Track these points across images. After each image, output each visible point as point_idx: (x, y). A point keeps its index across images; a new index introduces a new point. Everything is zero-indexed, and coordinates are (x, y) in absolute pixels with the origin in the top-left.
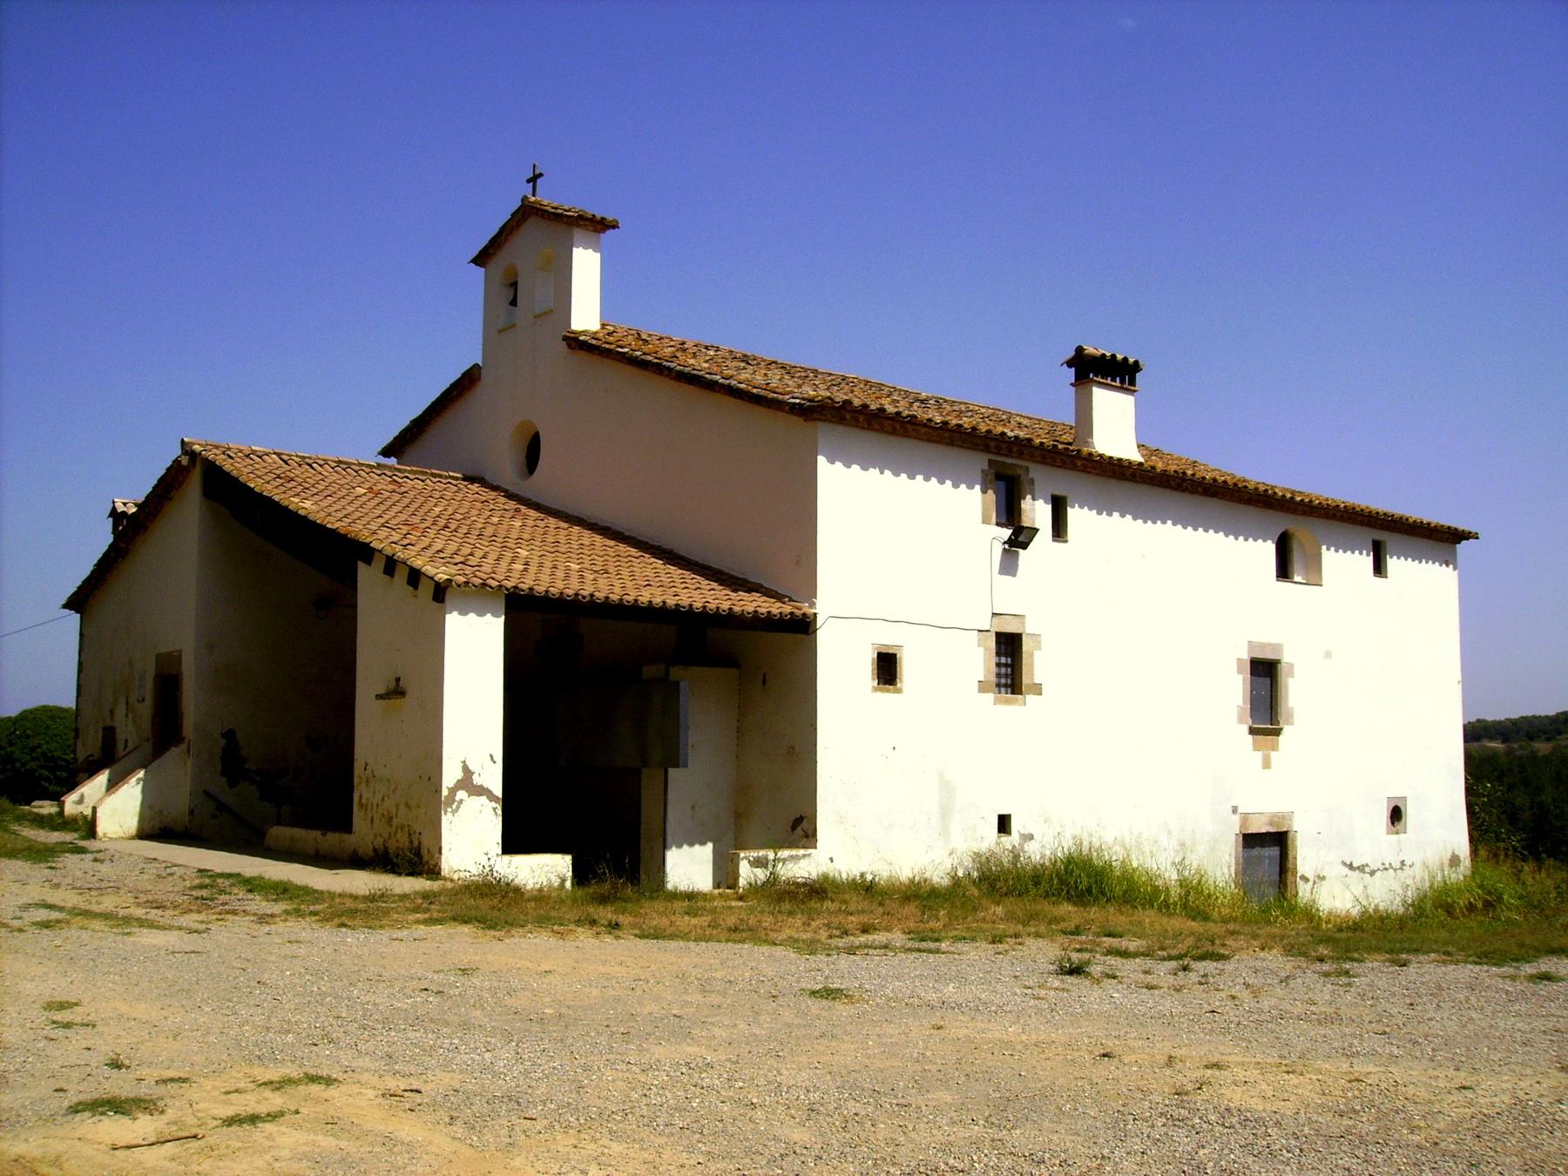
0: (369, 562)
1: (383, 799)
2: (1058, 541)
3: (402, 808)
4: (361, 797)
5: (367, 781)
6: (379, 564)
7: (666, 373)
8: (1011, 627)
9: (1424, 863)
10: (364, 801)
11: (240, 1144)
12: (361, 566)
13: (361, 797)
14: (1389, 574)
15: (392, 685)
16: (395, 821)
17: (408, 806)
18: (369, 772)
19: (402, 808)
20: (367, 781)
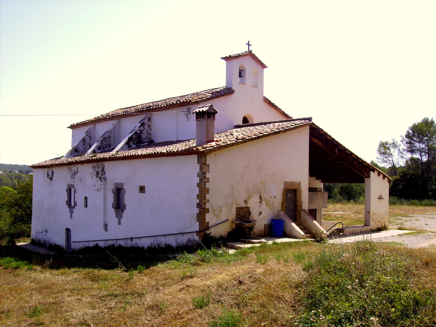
0: (374, 171)
1: (378, 218)
2: (293, 183)
3: (382, 219)
4: (372, 218)
5: (374, 215)
6: (376, 172)
7: (142, 157)
8: (120, 187)
9: (261, 203)
10: (373, 219)
11: (71, 294)
12: (371, 172)
13: (372, 218)
14: (144, 185)
15: (379, 197)
16: (380, 222)
17: (383, 218)
18: (374, 213)
19: (382, 219)
20: (374, 215)
